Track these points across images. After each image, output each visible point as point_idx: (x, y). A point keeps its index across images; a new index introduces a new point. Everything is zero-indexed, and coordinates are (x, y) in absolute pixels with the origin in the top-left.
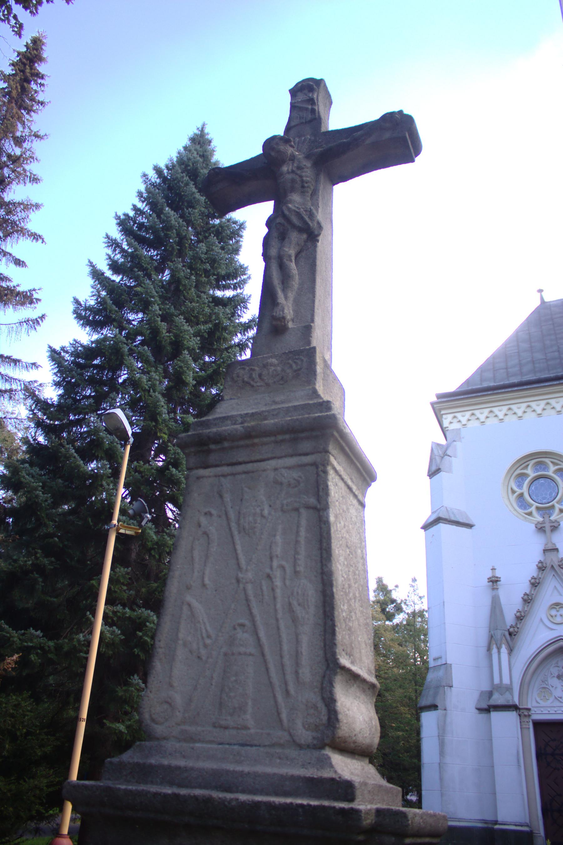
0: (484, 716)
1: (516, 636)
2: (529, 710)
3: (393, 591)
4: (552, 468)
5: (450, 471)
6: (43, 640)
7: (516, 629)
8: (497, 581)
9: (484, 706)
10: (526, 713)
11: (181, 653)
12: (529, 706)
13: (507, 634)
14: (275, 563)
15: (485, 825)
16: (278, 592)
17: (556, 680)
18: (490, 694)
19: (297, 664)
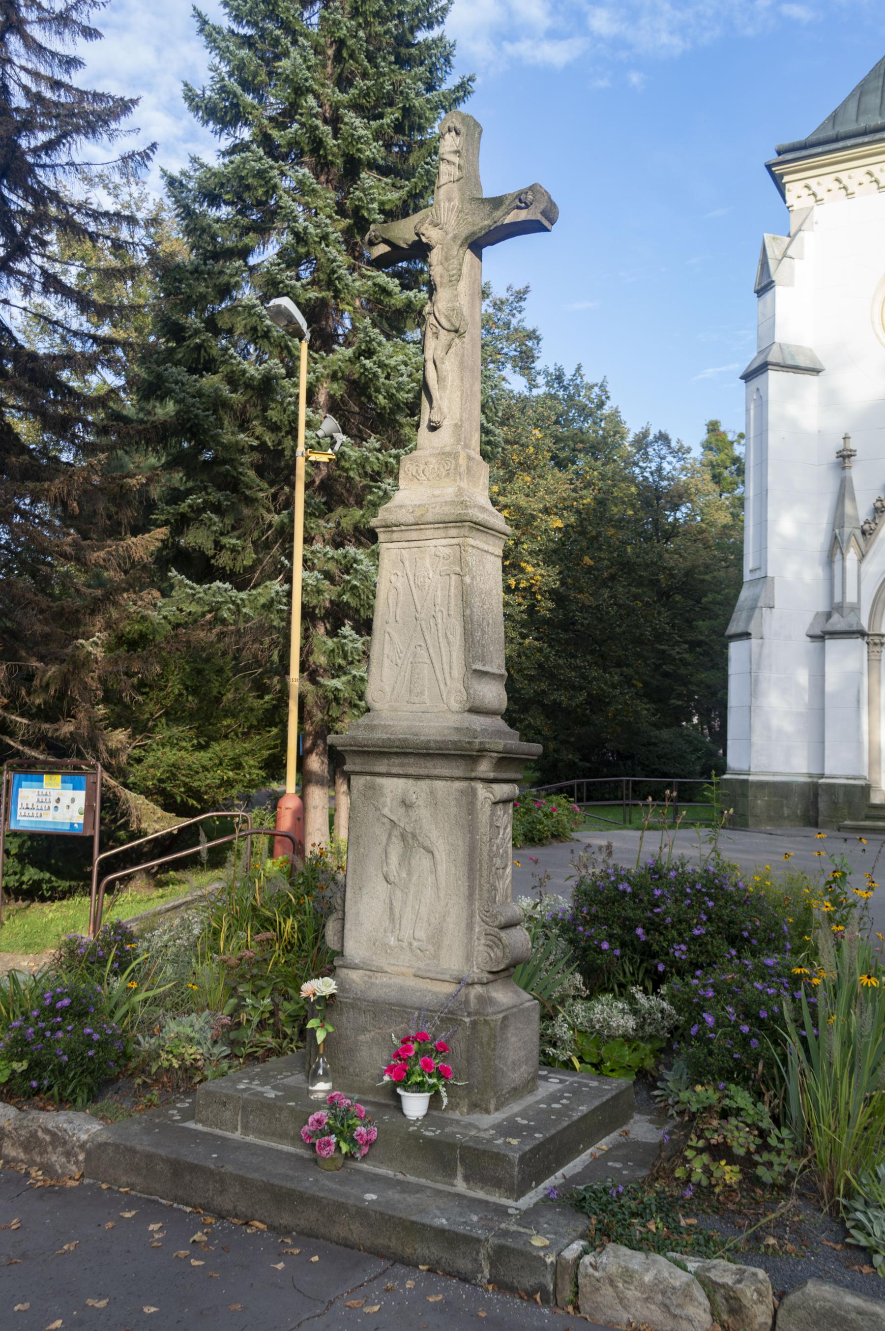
0: (817, 644)
3: (735, 445)
5: (790, 283)
6: (234, 593)
7: (873, 526)
8: (849, 456)
9: (817, 632)
10: (877, 641)
11: (386, 662)
13: (858, 532)
14: (437, 608)
15: (809, 780)
16: (440, 626)
18: (829, 615)
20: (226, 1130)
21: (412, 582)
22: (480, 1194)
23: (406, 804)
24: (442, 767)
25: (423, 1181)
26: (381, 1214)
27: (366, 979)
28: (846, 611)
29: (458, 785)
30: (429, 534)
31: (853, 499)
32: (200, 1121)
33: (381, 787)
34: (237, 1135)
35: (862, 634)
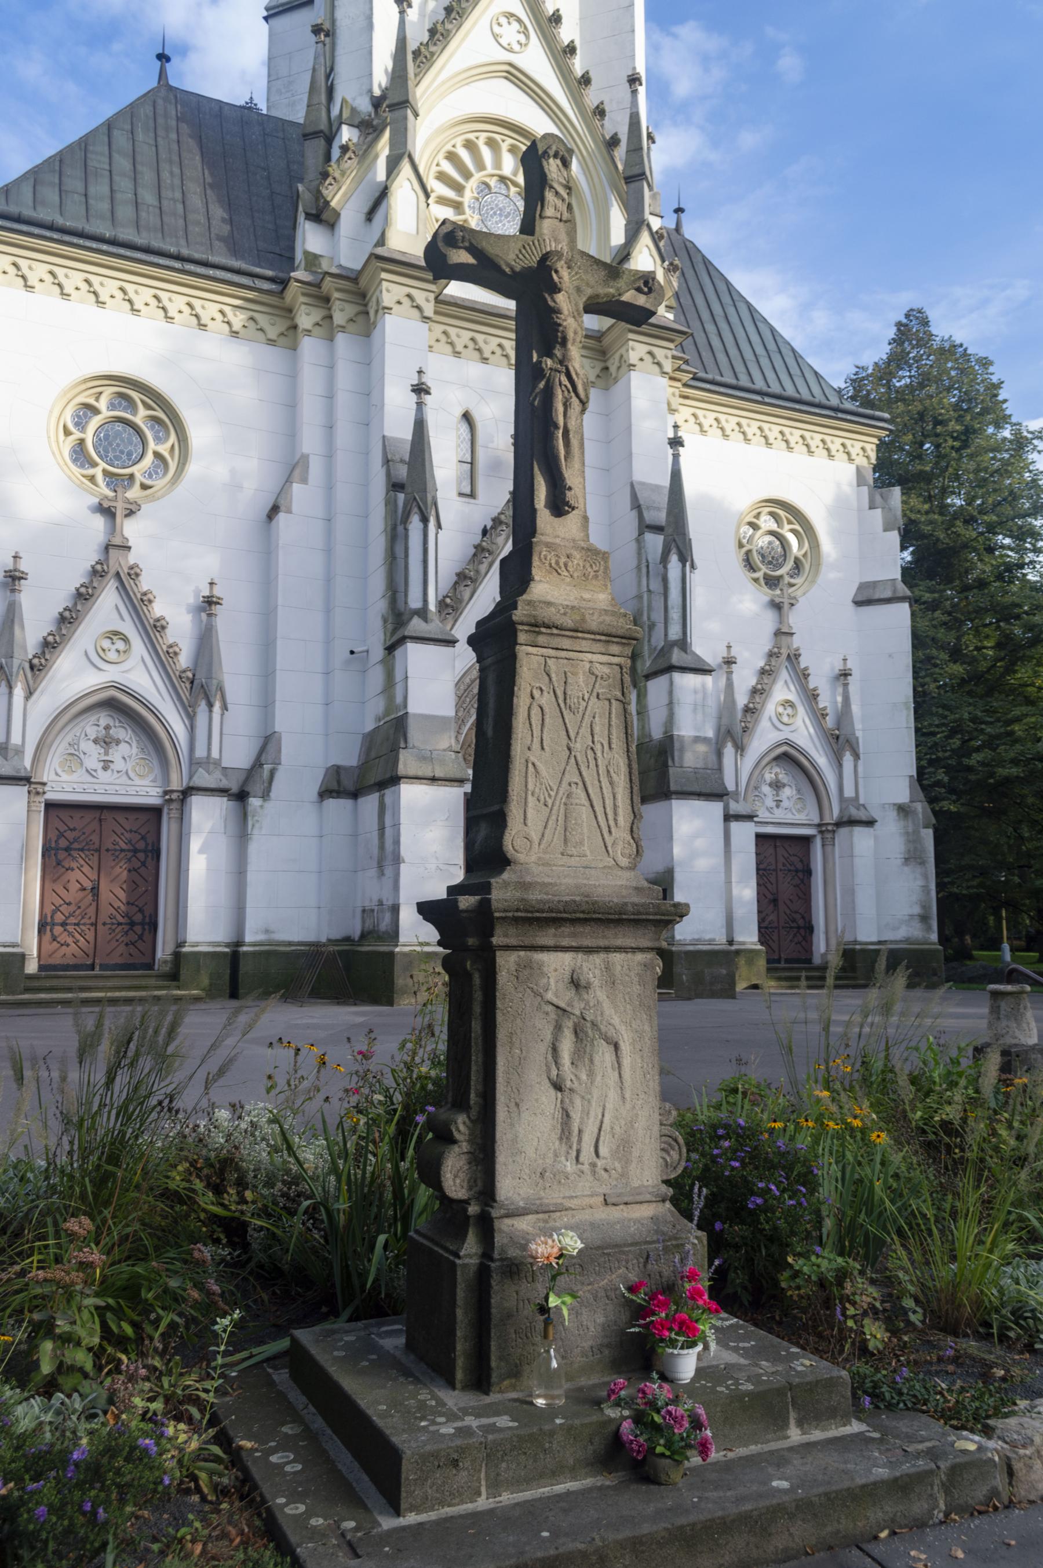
1: (43, 673)
2: (44, 784)
4: (142, 412)
12: (45, 780)
13: (27, 666)
17: (91, 743)
19: (615, 814)
20: (462, 1502)
21: (561, 701)
22: (817, 1435)
23: (576, 983)
24: (624, 936)
25: (754, 1449)
26: (826, 1494)
27: (541, 1224)
28: (11, 754)
29: (640, 957)
30: (585, 645)
31: (22, 627)
32: (412, 1508)
33: (541, 965)
34: (483, 1503)
35: (26, 780)
